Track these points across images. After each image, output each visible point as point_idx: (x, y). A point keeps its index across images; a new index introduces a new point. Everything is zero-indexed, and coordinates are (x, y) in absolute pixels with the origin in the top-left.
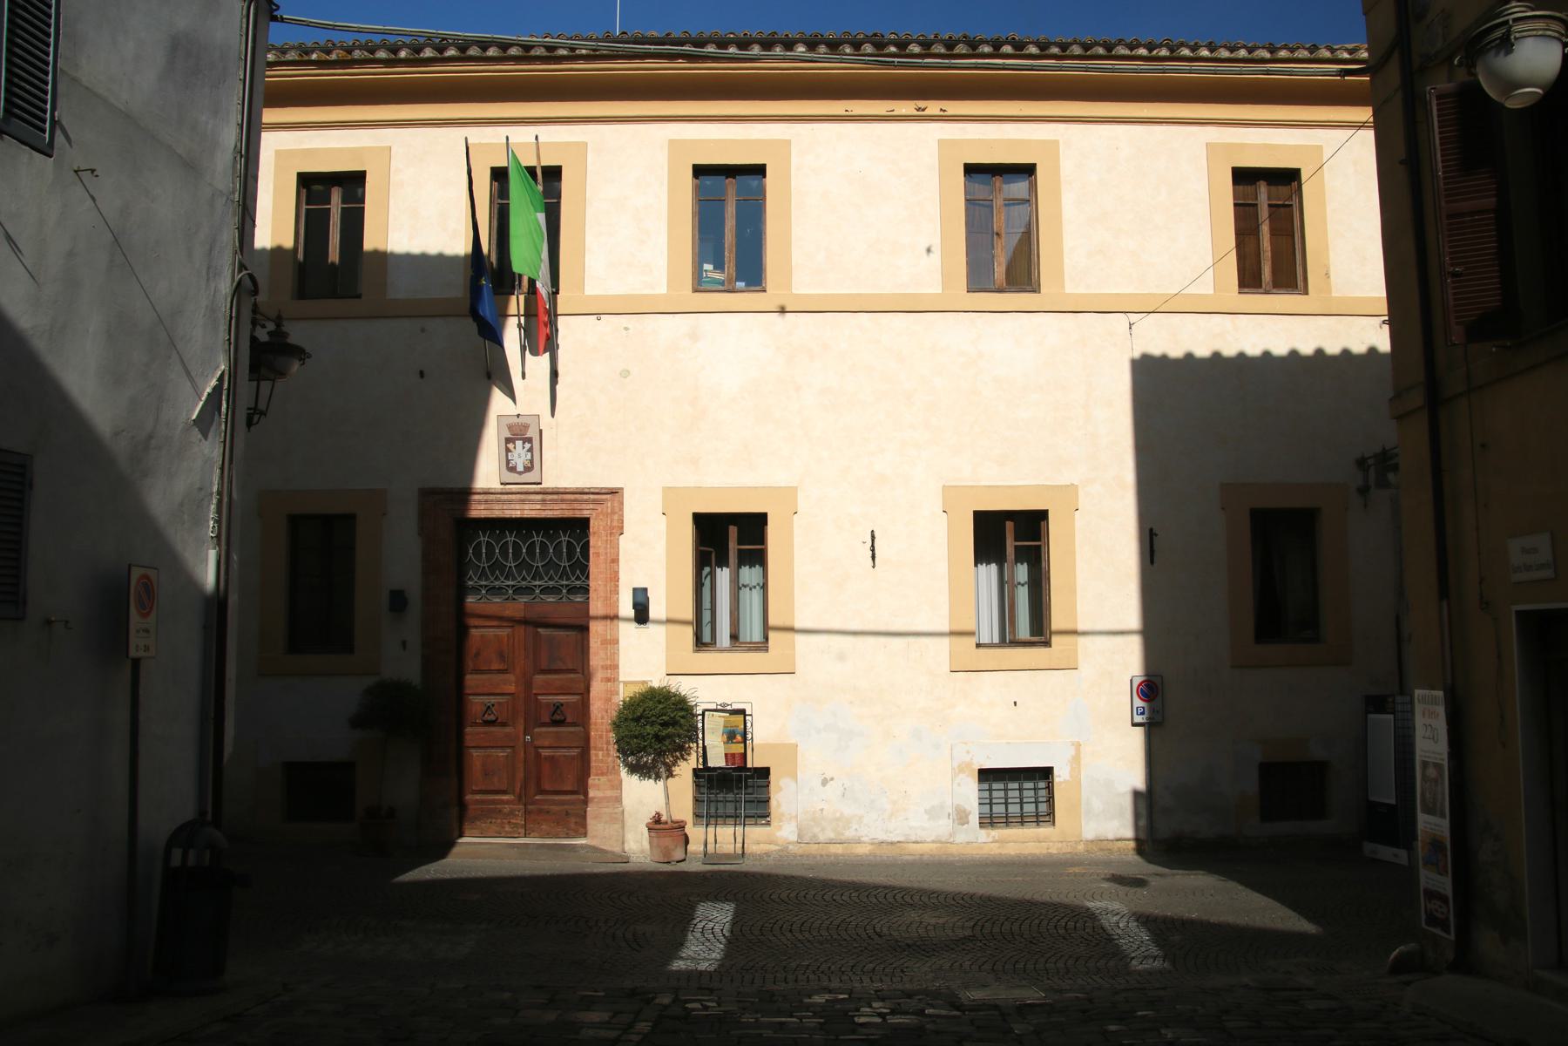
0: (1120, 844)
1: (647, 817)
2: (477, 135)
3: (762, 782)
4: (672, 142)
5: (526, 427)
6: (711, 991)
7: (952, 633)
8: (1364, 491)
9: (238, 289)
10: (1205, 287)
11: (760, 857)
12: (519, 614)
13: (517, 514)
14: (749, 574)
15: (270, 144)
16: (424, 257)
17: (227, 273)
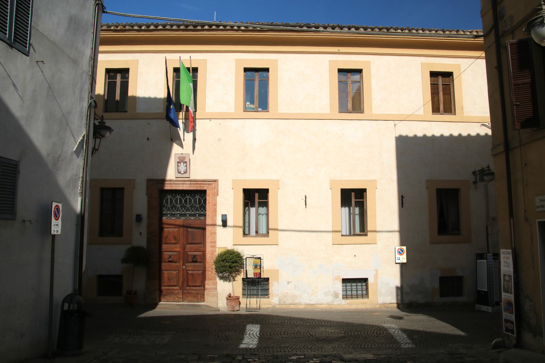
0: (391, 305)
1: (226, 295)
2: (169, 56)
3: (266, 283)
4: (236, 60)
5: (185, 158)
6: (255, 355)
7: (333, 231)
8: (475, 183)
9: (90, 106)
10: (421, 112)
11: (266, 309)
12: (181, 224)
13: (181, 188)
14: (262, 210)
15: (101, 57)
16: (150, 99)
17: (86, 100)
